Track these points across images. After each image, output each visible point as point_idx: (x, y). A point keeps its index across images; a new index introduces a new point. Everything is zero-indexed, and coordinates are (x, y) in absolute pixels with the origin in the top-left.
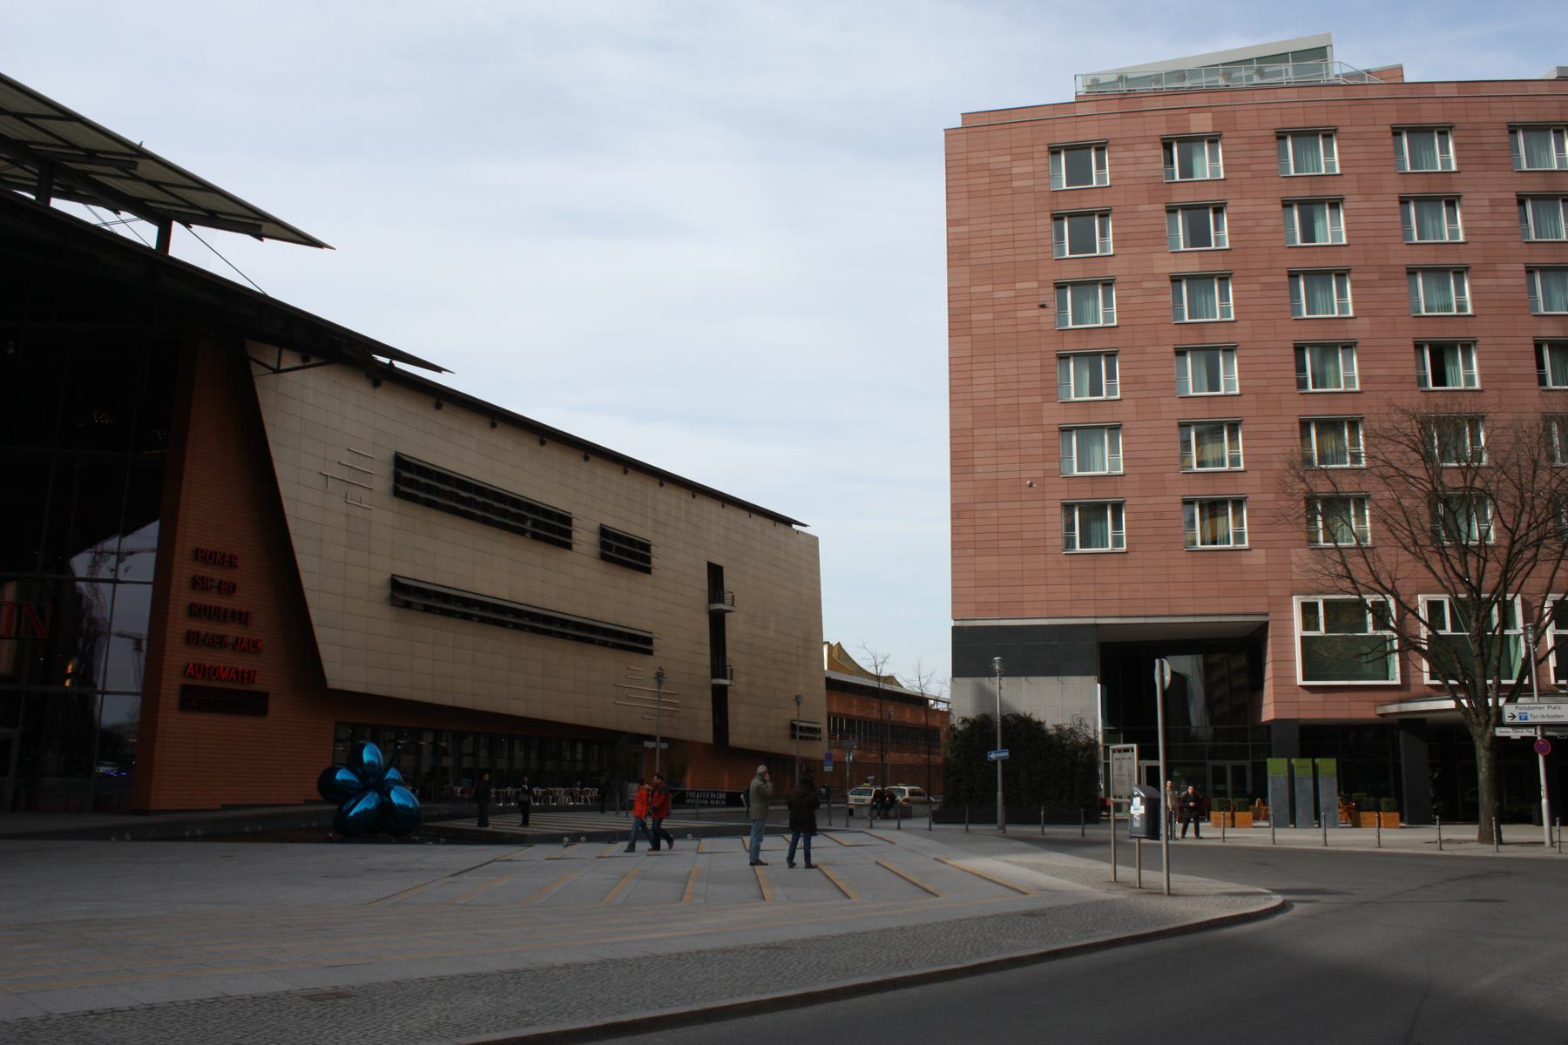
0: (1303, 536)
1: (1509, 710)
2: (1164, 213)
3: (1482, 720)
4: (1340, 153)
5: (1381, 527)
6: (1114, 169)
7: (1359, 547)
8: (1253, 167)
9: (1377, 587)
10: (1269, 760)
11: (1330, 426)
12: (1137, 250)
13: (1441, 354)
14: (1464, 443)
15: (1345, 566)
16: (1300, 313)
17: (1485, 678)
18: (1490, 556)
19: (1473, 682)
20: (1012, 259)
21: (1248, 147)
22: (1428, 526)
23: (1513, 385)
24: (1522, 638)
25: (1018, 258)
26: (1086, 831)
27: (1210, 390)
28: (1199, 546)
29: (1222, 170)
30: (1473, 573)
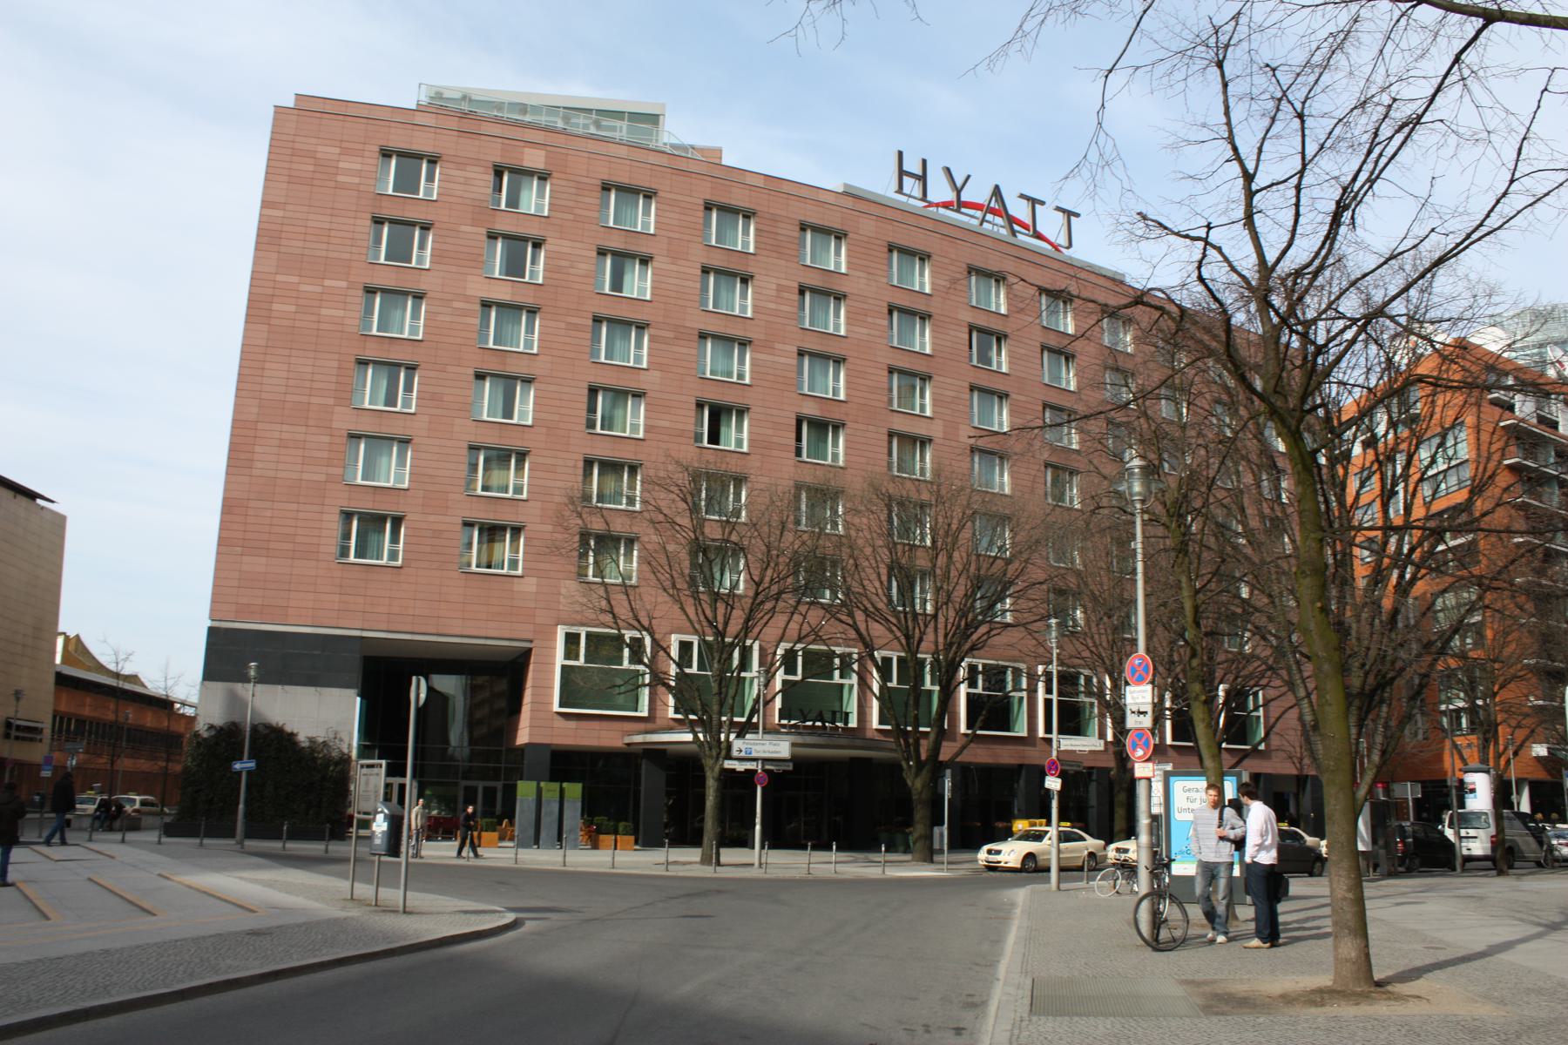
0: (575, 569)
1: (738, 745)
2: (485, 238)
3: (714, 753)
4: (656, 215)
5: (646, 568)
6: (443, 184)
7: (624, 585)
8: (577, 211)
9: (635, 623)
10: (519, 783)
11: (611, 467)
12: (453, 269)
13: (718, 414)
14: (727, 498)
15: (609, 602)
16: (487, 342)
17: (721, 714)
18: (737, 605)
19: (710, 718)
20: (324, 254)
21: (574, 191)
22: (687, 571)
23: (775, 453)
24: (756, 681)
25: (331, 255)
26: (330, 847)
27: (386, 405)
28: (474, 568)
29: (547, 208)
30: (720, 619)
